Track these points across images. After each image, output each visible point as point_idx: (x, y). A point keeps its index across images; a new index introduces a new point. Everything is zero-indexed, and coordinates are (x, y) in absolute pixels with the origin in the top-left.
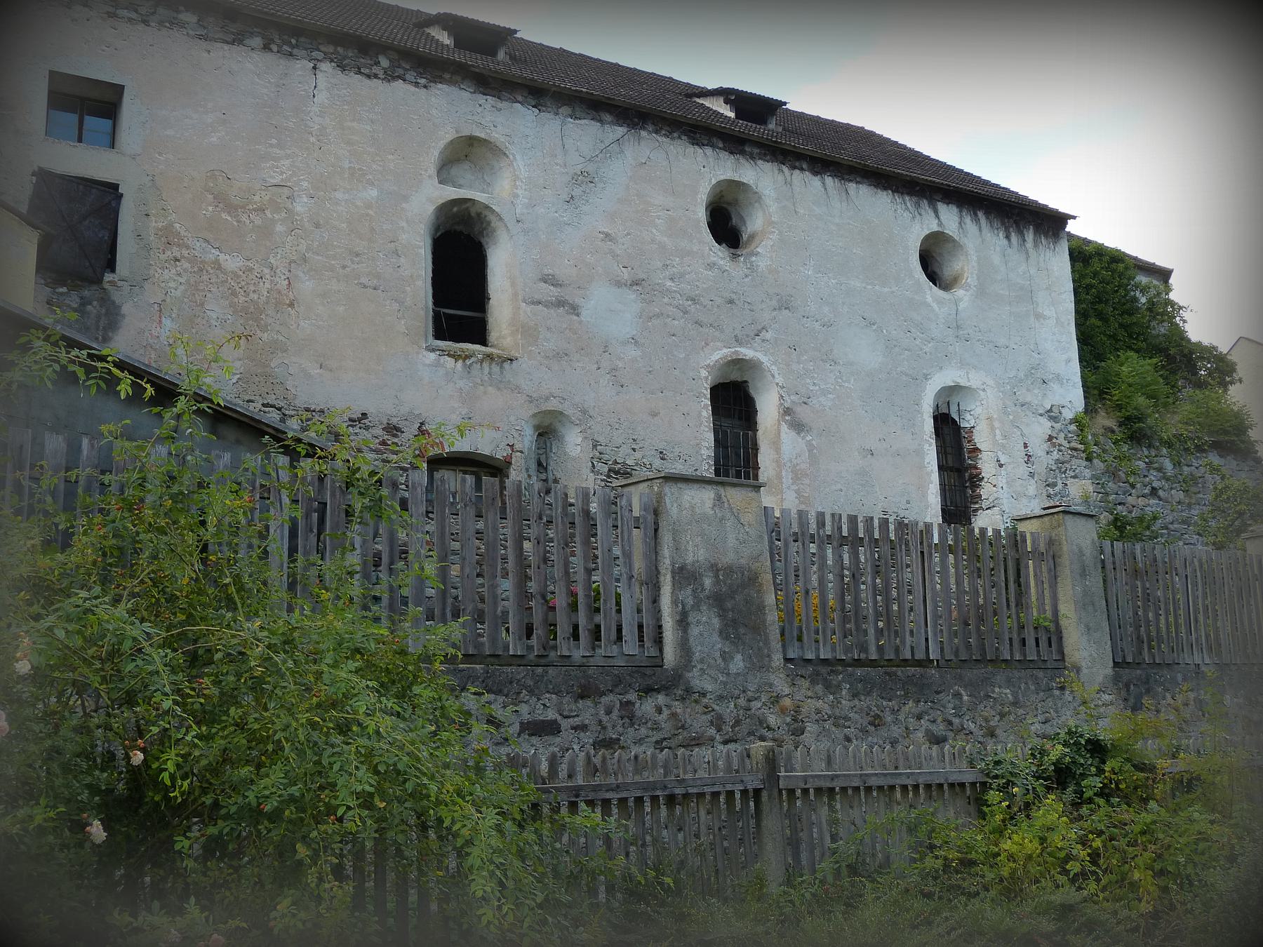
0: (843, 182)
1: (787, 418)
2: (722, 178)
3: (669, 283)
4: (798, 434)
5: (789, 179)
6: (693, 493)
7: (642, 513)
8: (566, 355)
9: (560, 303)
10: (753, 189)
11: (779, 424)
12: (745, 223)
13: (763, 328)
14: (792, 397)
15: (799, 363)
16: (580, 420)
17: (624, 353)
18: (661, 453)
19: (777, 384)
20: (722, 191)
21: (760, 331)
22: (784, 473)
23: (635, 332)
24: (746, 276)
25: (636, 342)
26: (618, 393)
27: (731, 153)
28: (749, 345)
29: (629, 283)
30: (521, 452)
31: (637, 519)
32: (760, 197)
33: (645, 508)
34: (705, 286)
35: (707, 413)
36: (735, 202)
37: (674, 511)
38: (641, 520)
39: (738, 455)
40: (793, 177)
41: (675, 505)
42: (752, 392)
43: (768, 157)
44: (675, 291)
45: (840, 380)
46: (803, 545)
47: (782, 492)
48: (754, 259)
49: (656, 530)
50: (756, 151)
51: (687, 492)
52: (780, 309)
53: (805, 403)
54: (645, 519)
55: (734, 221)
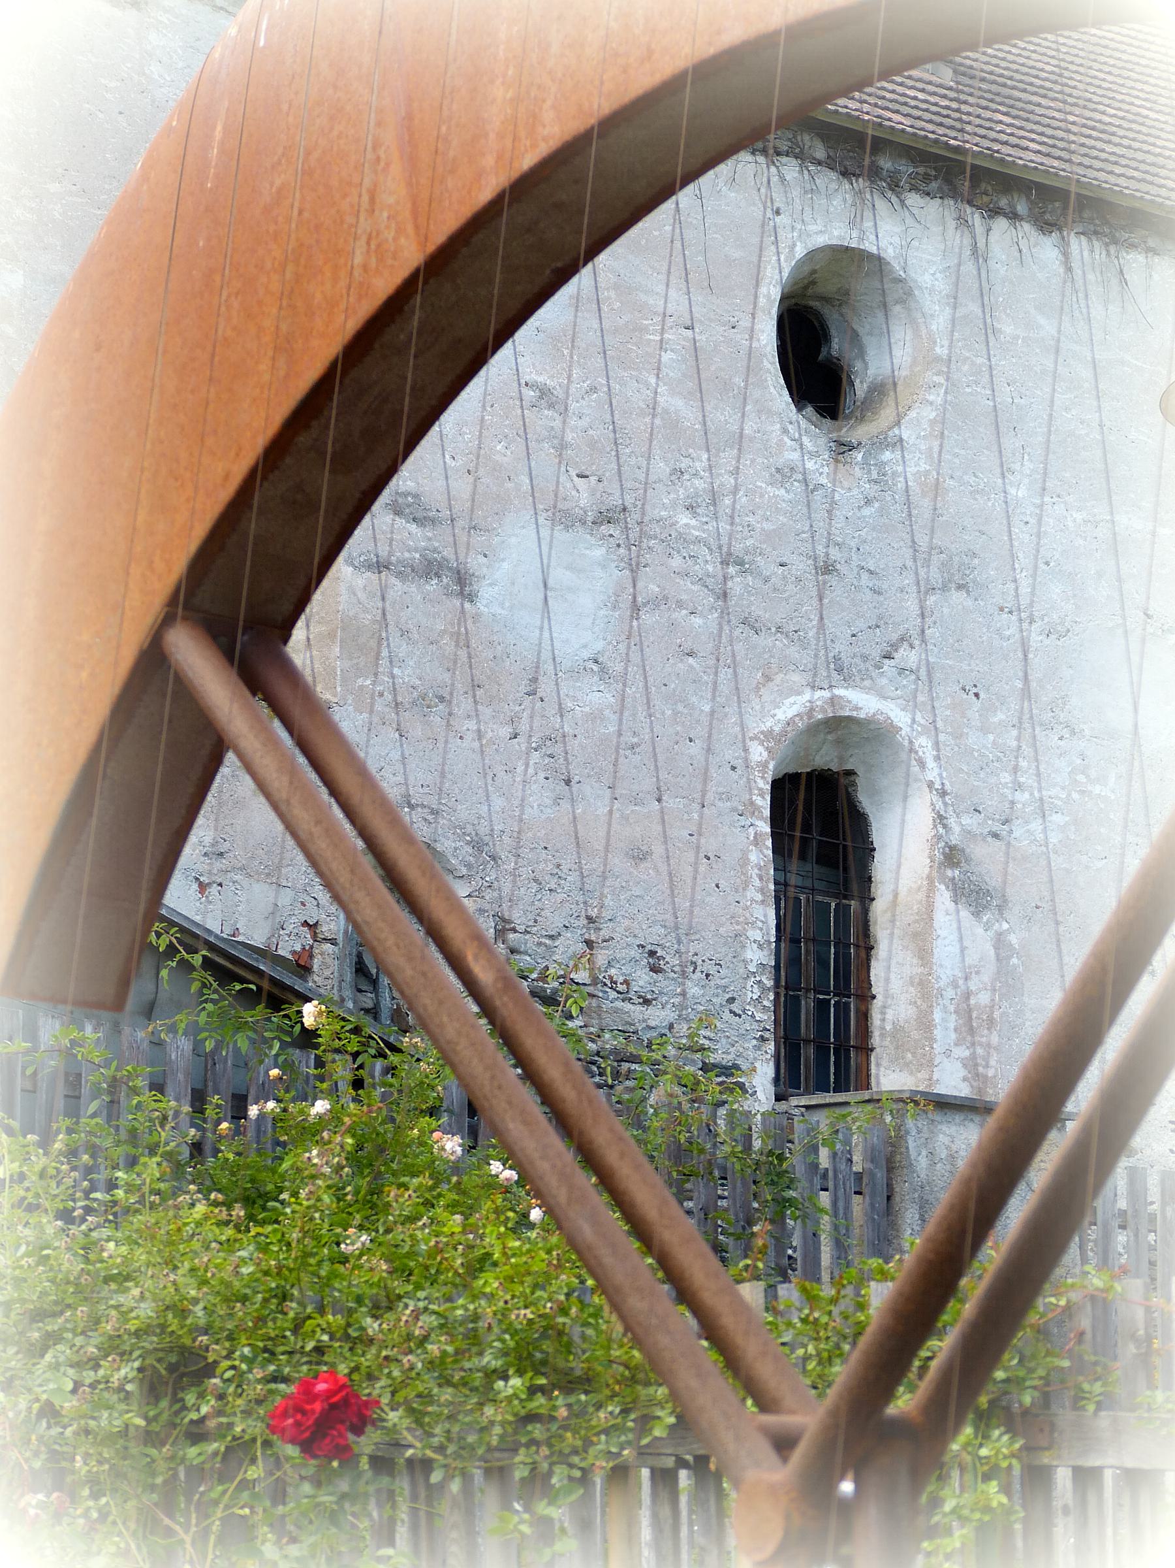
0: (1112, 249)
1: (949, 873)
2: (821, 240)
3: (684, 519)
4: (977, 914)
5: (981, 243)
6: (951, 1129)
7: (868, 1165)
8: (442, 699)
9: (430, 568)
10: (891, 271)
11: (931, 888)
12: (862, 354)
13: (902, 639)
14: (966, 820)
15: (985, 730)
16: (469, 866)
17: (574, 698)
18: (652, 953)
19: (930, 785)
20: (814, 272)
21: (895, 646)
22: (937, 1016)
23: (599, 645)
24: (868, 502)
25: (603, 670)
26: (557, 800)
27: (845, 174)
28: (867, 683)
29: (590, 517)
30: (333, 942)
31: (859, 1176)
32: (909, 293)
33: (872, 1156)
34: (767, 526)
35: (762, 855)
36: (841, 299)
37: (922, 1163)
38: (865, 1180)
39: (823, 963)
40: (994, 236)
41: (924, 1153)
42: (865, 801)
43: (934, 185)
44: (698, 541)
45: (1081, 778)
46: (1136, 1235)
47: (931, 1064)
48: (887, 455)
49: (889, 1198)
50: (906, 169)
51: (944, 1128)
52: (944, 588)
53: (996, 836)
54: (872, 1175)
55: (837, 346)
